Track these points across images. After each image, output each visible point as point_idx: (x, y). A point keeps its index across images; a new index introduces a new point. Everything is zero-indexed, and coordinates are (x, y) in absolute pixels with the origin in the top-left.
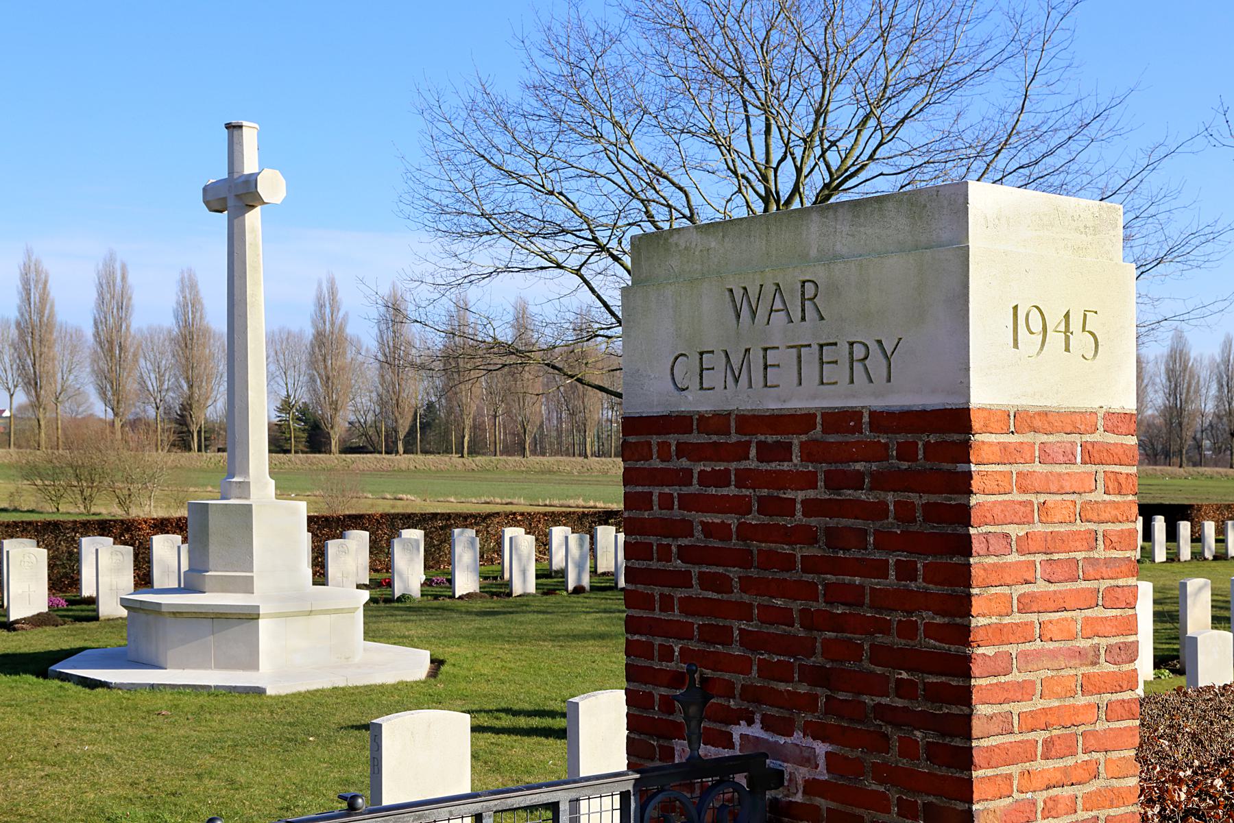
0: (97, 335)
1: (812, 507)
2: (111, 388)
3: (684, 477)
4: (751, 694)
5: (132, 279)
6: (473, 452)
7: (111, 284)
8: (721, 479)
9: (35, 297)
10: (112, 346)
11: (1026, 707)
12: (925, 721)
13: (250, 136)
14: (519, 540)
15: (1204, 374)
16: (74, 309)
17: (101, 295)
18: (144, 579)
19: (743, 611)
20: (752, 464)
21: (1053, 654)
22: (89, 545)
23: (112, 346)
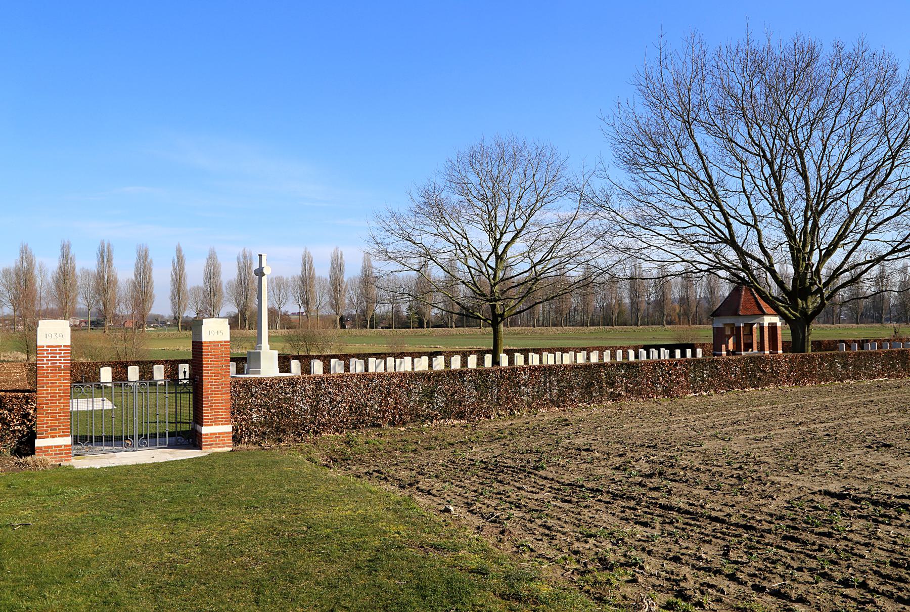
6: (372, 327)
7: (336, 260)
10: (336, 286)
14: (643, 352)
15: (224, 284)
16: (322, 272)
17: (333, 265)
23: (336, 286)
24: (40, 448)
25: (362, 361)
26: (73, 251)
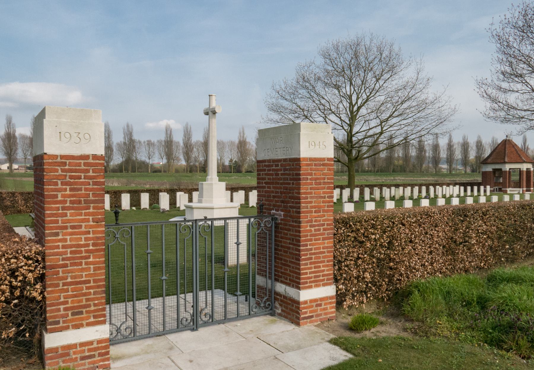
0: (184, 144)
1: (282, 174)
2: (188, 157)
3: (265, 170)
4: (274, 206)
5: (192, 129)
8: (269, 170)
9: (169, 132)
11: (311, 205)
12: (294, 207)
13: (214, 98)
15: (115, 144)
16: (178, 138)
18: (190, 200)
19: (273, 192)
20: (274, 168)
21: (317, 197)
22: (178, 194)
24: (55, 350)
25: (187, 195)
26: (14, 121)
